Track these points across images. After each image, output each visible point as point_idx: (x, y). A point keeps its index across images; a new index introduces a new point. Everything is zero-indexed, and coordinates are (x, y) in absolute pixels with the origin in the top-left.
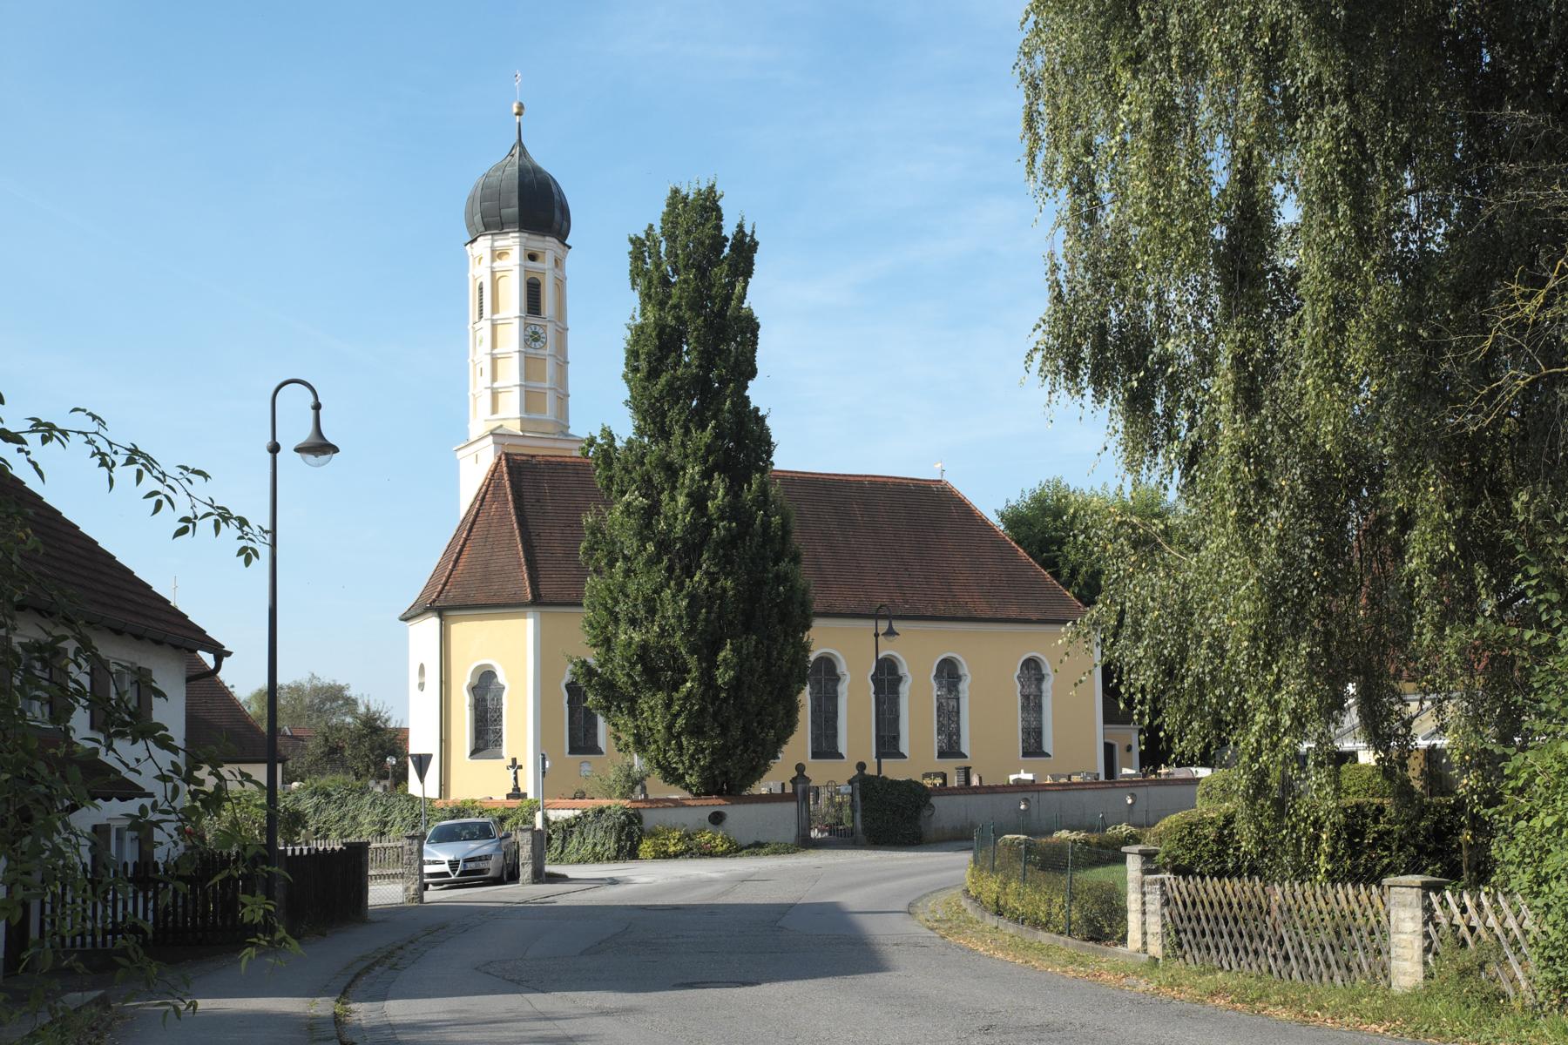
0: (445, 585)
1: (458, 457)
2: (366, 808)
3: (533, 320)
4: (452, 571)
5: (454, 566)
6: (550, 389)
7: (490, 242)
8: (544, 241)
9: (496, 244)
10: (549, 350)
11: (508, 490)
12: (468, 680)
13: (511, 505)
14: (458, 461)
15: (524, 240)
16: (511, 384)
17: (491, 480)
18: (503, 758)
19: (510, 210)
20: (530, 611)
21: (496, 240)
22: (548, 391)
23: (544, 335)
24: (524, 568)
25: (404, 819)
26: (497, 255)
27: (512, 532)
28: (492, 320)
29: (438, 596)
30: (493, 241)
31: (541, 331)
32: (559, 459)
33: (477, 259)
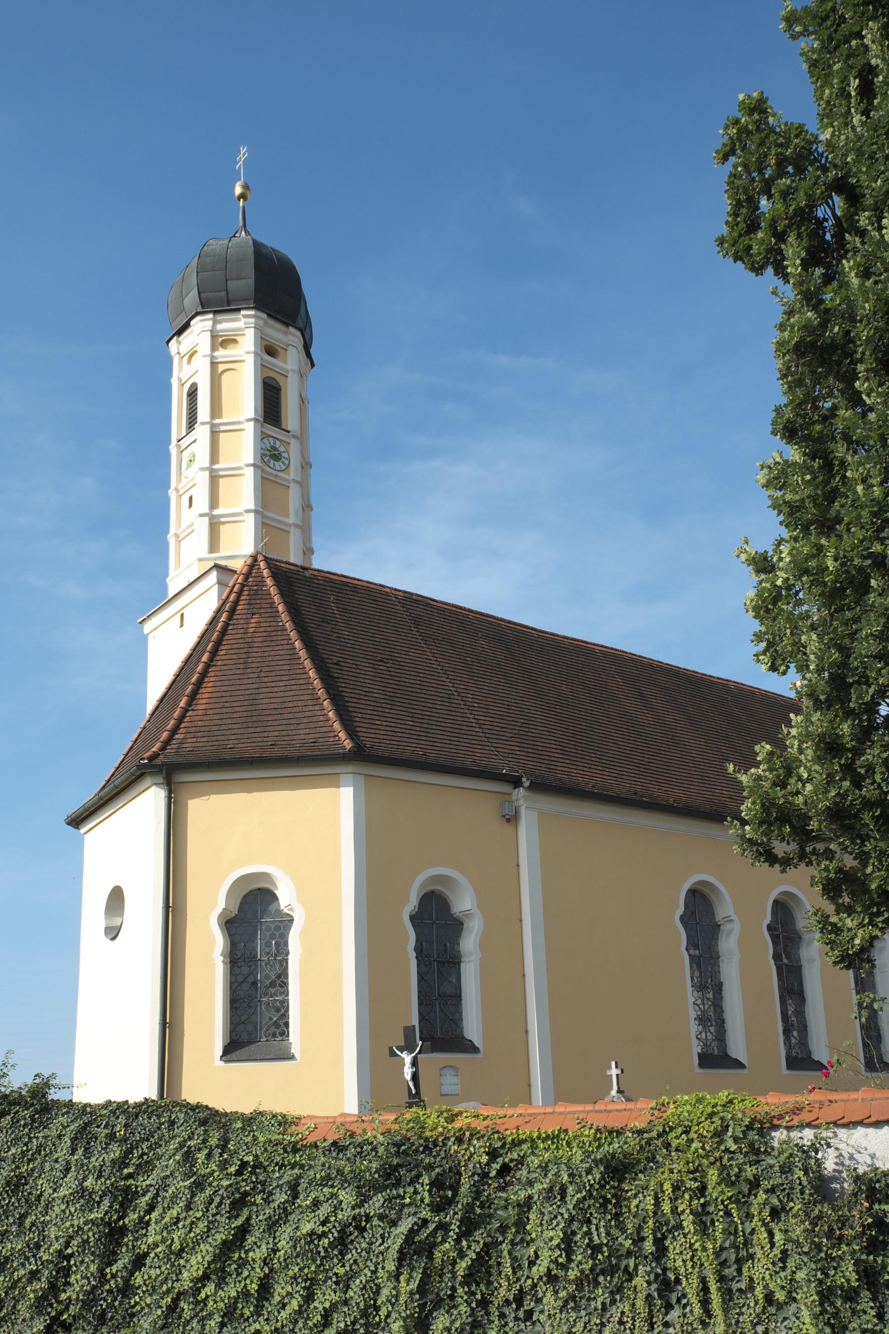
0: (174, 731)
1: (146, 632)
2: (62, 1152)
3: (271, 430)
4: (185, 711)
5: (189, 704)
6: (295, 525)
7: (210, 323)
8: (286, 333)
9: (219, 327)
10: (293, 473)
11: (277, 599)
12: (221, 905)
13: (285, 617)
14: (145, 638)
15: (261, 323)
16: (240, 509)
17: (243, 586)
18: (292, 1058)
19: (241, 283)
20: (347, 772)
21: (220, 322)
22: (292, 530)
23: (285, 455)
24: (326, 703)
25: (199, 1185)
26: (220, 341)
27: (293, 655)
28: (213, 426)
29: (163, 749)
30: (215, 322)
31: (282, 449)
32: (344, 579)
33: (186, 359)
